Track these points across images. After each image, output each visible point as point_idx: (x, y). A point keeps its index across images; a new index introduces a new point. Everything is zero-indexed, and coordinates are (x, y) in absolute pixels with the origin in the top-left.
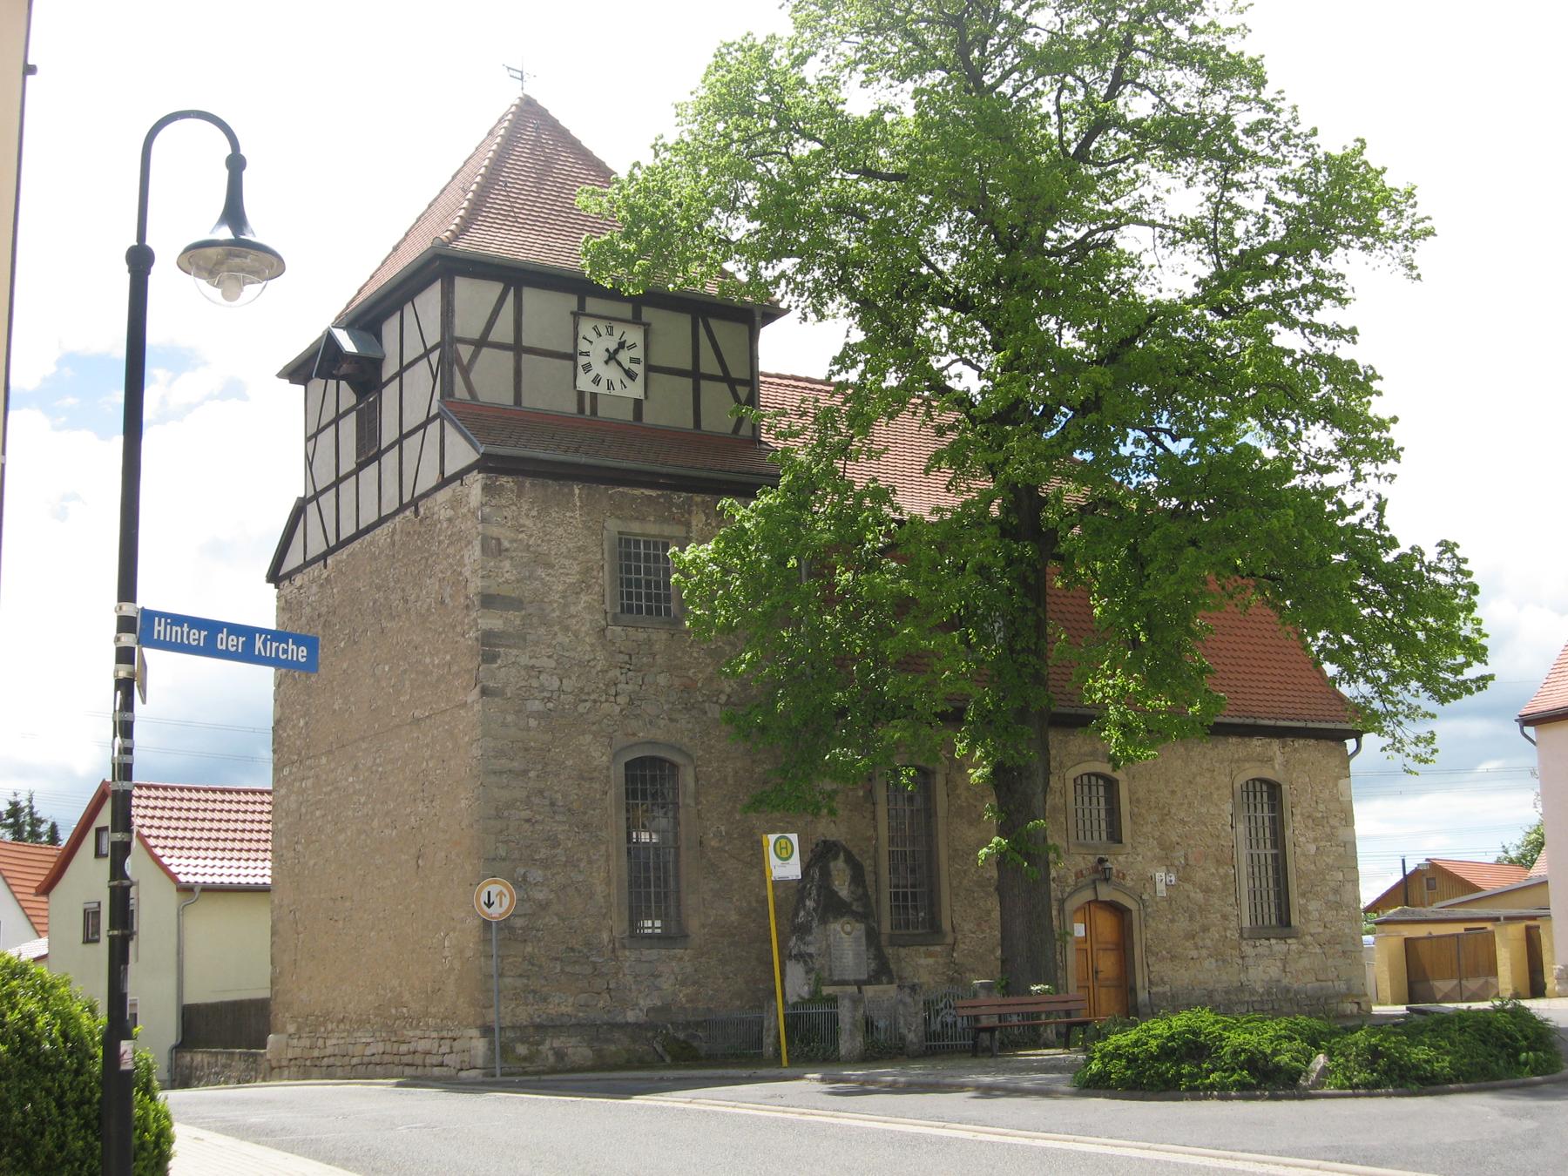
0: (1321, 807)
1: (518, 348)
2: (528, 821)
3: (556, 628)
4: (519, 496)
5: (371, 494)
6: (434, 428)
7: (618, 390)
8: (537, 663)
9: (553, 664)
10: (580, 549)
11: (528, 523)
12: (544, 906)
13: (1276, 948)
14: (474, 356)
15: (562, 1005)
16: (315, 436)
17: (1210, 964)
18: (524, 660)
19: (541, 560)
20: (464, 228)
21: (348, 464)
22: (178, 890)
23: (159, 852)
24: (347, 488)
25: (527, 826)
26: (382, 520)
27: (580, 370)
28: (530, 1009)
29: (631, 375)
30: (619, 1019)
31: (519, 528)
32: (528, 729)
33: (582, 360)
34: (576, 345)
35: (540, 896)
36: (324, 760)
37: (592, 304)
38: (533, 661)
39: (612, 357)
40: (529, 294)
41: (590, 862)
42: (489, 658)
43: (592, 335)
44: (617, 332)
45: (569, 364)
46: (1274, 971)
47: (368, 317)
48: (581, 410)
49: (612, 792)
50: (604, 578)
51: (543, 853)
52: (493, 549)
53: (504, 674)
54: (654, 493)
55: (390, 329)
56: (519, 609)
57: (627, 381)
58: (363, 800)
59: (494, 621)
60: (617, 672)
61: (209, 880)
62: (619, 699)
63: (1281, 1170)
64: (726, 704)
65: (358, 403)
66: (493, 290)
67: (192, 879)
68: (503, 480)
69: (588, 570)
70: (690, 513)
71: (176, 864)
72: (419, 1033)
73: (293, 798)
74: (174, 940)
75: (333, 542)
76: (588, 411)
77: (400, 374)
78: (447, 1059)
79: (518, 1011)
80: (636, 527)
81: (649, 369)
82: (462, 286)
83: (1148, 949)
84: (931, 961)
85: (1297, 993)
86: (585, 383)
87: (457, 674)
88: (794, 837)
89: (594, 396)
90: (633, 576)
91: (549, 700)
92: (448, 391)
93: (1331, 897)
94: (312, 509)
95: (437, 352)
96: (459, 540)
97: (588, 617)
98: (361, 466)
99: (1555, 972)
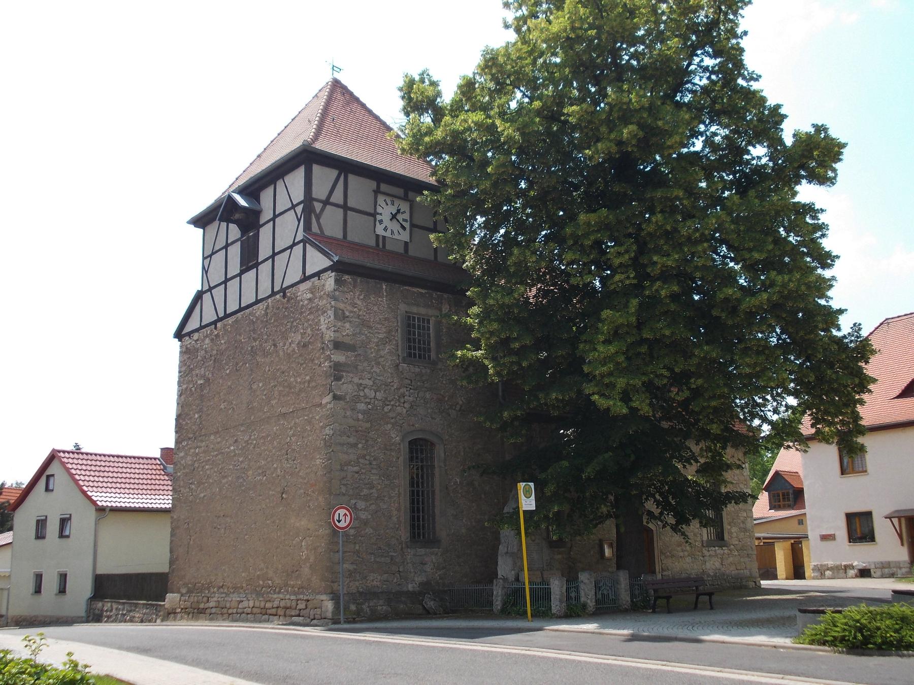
0: (736, 478)
1: (345, 207)
2: (357, 473)
3: (373, 363)
4: (354, 287)
5: (250, 287)
6: (299, 249)
7: (396, 236)
8: (364, 382)
9: (371, 383)
10: (386, 319)
11: (359, 302)
12: (366, 523)
13: (718, 552)
14: (323, 210)
15: (375, 580)
16: (210, 256)
17: (688, 559)
18: (356, 380)
19: (364, 324)
20: (316, 136)
21: (234, 268)
22: (96, 510)
23: (85, 488)
24: (233, 285)
25: (356, 475)
26: (258, 302)
27: (377, 223)
28: (357, 583)
29: (404, 228)
30: (405, 589)
31: (354, 305)
32: (358, 420)
33: (379, 217)
34: (375, 209)
35: (363, 517)
36: (212, 437)
37: (384, 187)
38: (361, 381)
39: (394, 217)
40: (351, 177)
41: (390, 497)
42: (338, 378)
43: (383, 204)
44: (396, 204)
45: (372, 218)
46: (718, 565)
47: (254, 188)
48: (377, 244)
49: (401, 458)
50: (398, 336)
51: (365, 492)
52: (340, 316)
53: (346, 388)
54: (423, 291)
55: (266, 196)
56: (354, 351)
57: (401, 230)
58: (241, 459)
59: (339, 357)
60: (405, 389)
61: (114, 505)
62: (405, 405)
63: (792, 683)
64: (460, 410)
65: (242, 236)
66: (333, 173)
67: (105, 504)
68: (346, 277)
69: (389, 332)
70: (442, 303)
71: (95, 496)
72: (281, 596)
73: (189, 458)
74: (92, 538)
75: (221, 314)
76: (381, 246)
77: (273, 219)
78: (302, 613)
79: (351, 584)
80: (415, 309)
81: (413, 226)
82: (316, 169)
83: (661, 552)
84: (560, 556)
85: (728, 576)
86: (379, 230)
87: (315, 387)
88: (532, 484)
89: (384, 237)
90: (412, 337)
91: (369, 403)
92: (308, 228)
93: (742, 525)
94: (207, 297)
95: (301, 206)
96: (317, 311)
97: (390, 358)
98: (242, 272)
99: (812, 567)
